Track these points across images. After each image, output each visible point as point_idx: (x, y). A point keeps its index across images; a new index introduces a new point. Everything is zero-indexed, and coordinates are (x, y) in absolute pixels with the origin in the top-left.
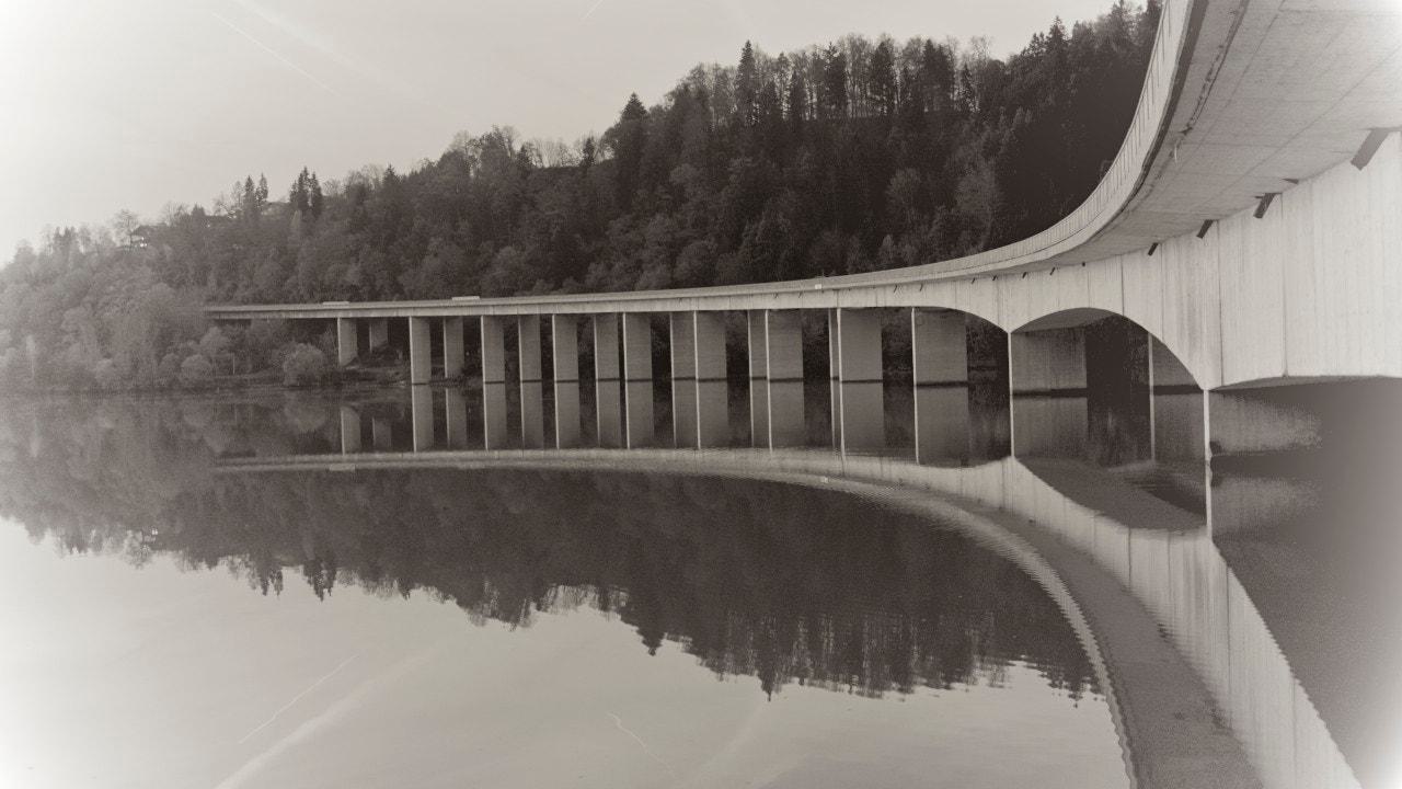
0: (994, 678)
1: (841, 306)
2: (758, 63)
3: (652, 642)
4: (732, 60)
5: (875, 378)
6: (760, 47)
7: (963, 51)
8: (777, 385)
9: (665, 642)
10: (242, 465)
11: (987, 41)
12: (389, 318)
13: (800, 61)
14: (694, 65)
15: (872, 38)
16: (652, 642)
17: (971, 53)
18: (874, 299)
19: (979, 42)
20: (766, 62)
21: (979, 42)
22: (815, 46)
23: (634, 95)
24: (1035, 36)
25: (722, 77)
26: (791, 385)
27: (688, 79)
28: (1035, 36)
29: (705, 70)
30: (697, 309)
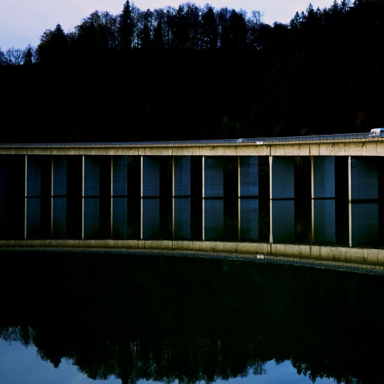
0: (256, 369)
1: (273, 154)
2: (133, 15)
3: (56, 363)
4: (117, 11)
5: (290, 197)
6: (175, 7)
7: (111, 14)
8: (208, 201)
9: (63, 360)
10: (15, 246)
11: (261, 14)
12: (260, 157)
13: (160, 14)
14: (92, 11)
15: (201, 5)
16: (56, 363)
17: (252, 19)
18: (137, 152)
19: (257, 14)
20: (139, 14)
21: (257, 14)
22: (169, 7)
23: (59, 25)
24: (297, 13)
25: (113, 20)
26: (217, 201)
27: (89, 19)
28: (297, 13)
29: (100, 14)
30: (144, 154)
